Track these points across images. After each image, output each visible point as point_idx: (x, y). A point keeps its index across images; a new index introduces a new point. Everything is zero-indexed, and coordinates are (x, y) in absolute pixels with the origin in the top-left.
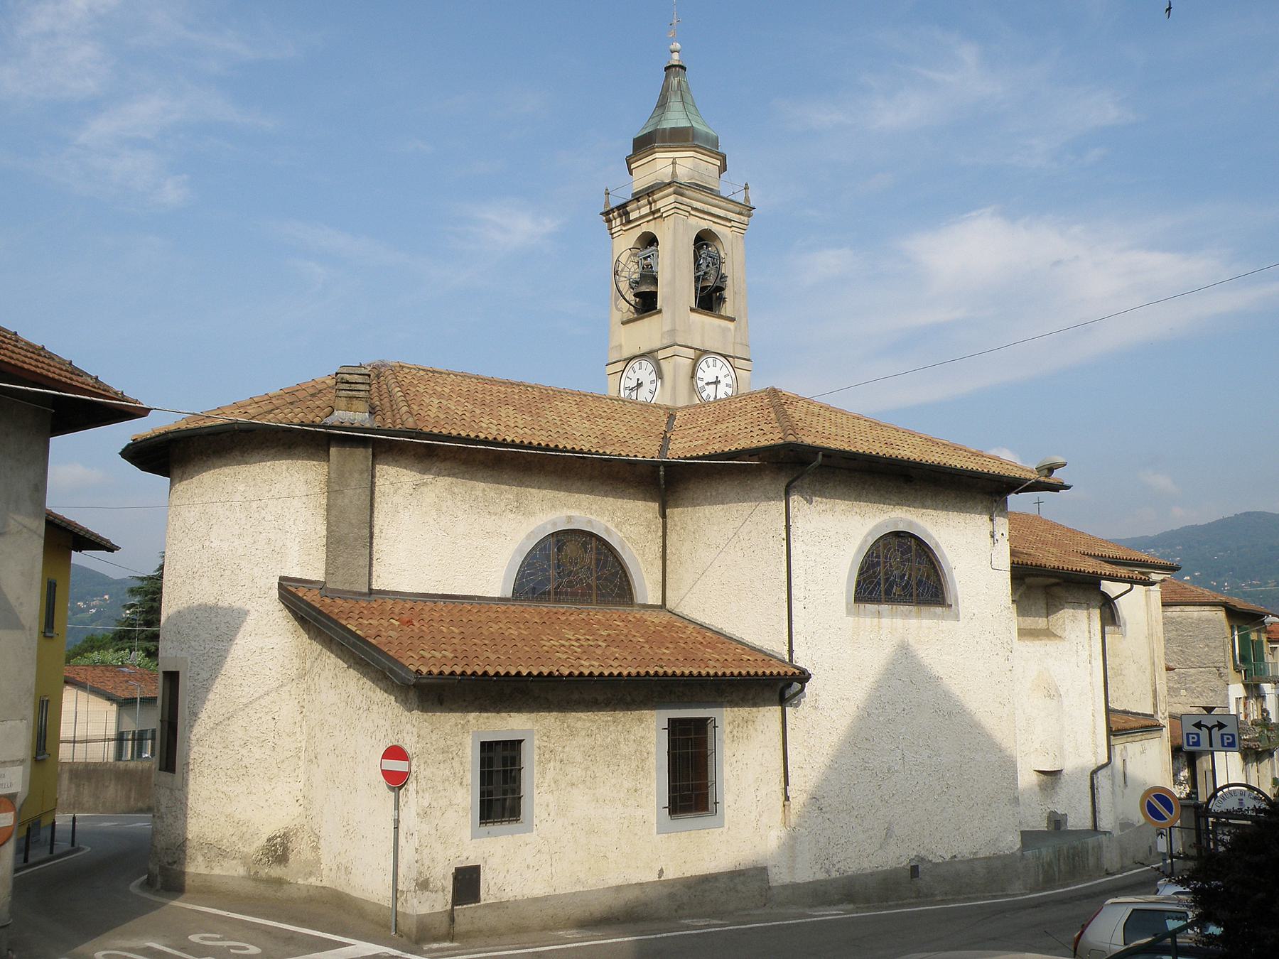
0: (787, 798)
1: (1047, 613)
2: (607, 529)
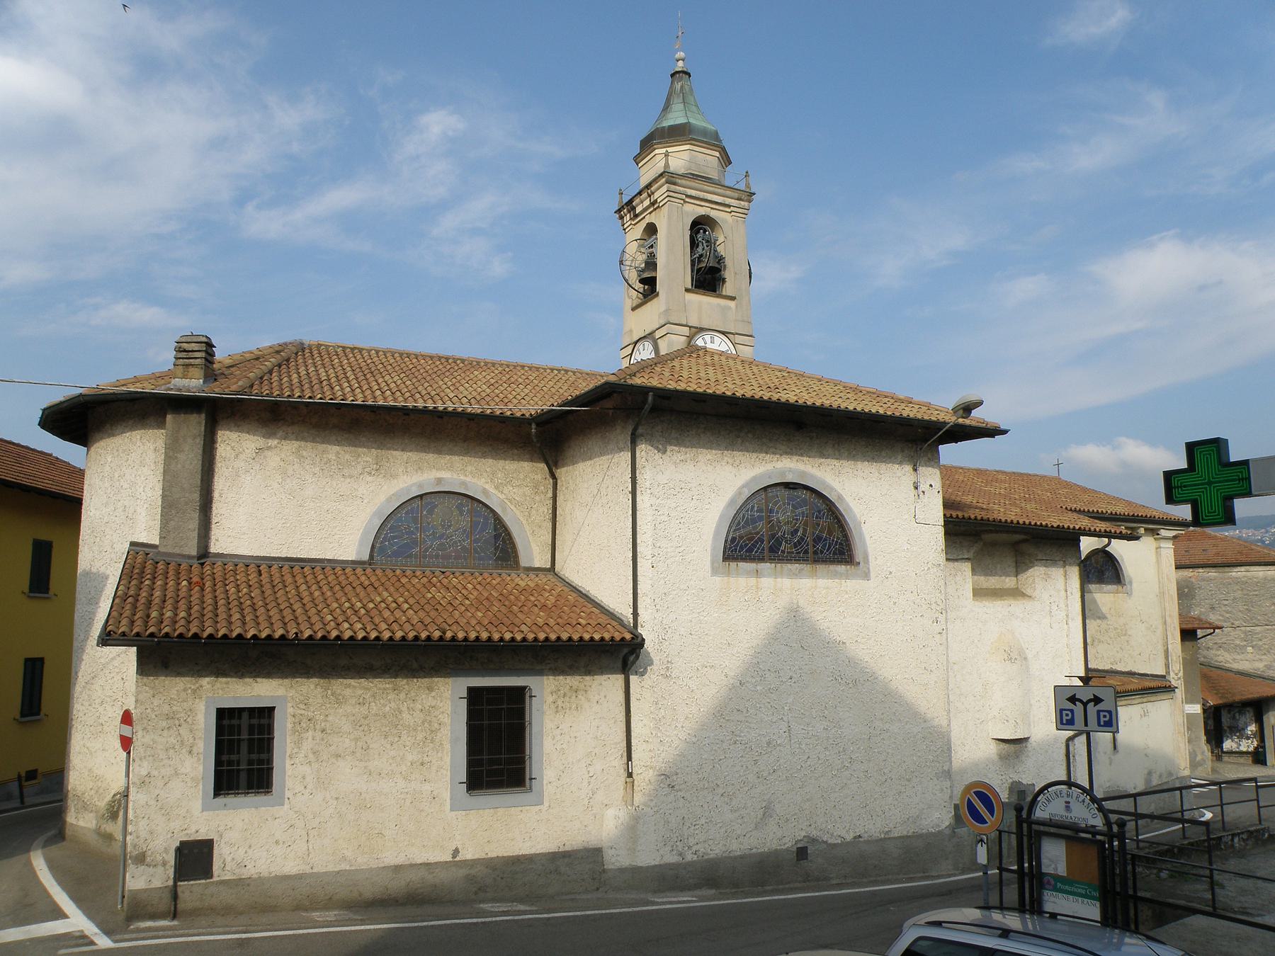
0: (630, 775)
1: (1017, 571)
2: (485, 491)
